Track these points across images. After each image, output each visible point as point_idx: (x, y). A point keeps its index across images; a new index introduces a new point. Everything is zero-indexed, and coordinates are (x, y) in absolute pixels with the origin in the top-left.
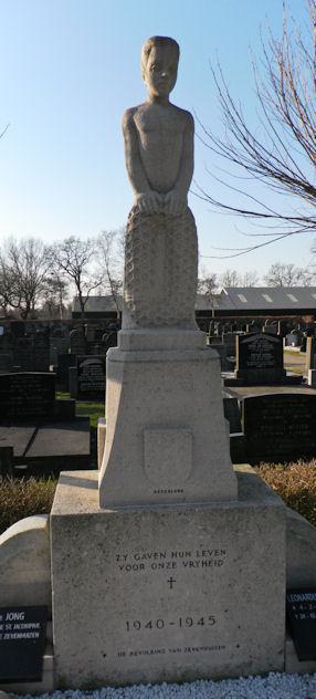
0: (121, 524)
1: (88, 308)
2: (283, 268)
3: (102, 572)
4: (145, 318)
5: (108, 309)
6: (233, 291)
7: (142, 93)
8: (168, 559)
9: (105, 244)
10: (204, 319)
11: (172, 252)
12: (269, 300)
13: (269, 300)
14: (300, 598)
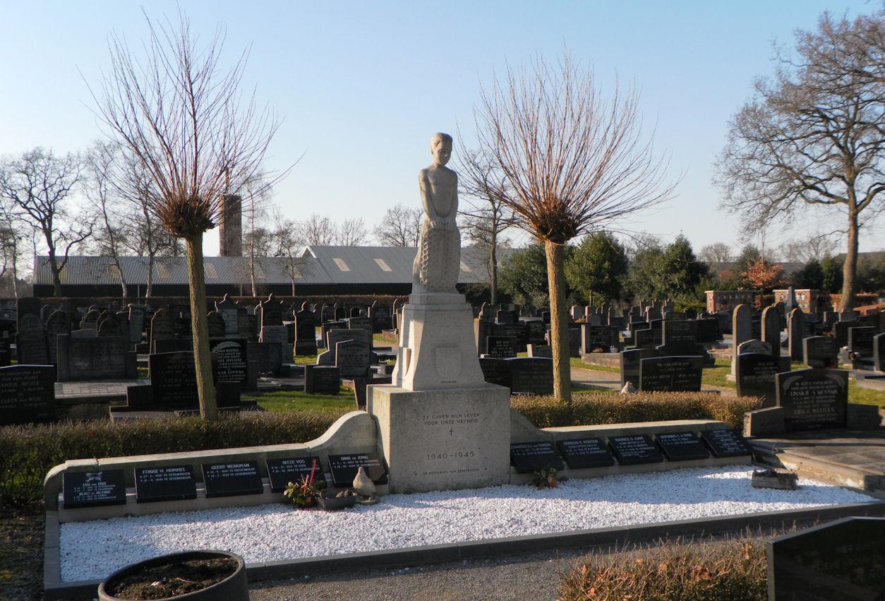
0: (426, 399)
1: (66, 278)
2: (407, 214)
3: (416, 425)
4: (432, 286)
5: (105, 280)
6: (327, 253)
7: (432, 161)
8: (450, 418)
9: (99, 163)
10: (461, 288)
11: (448, 250)
12: (386, 268)
13: (386, 268)
14: (515, 447)
